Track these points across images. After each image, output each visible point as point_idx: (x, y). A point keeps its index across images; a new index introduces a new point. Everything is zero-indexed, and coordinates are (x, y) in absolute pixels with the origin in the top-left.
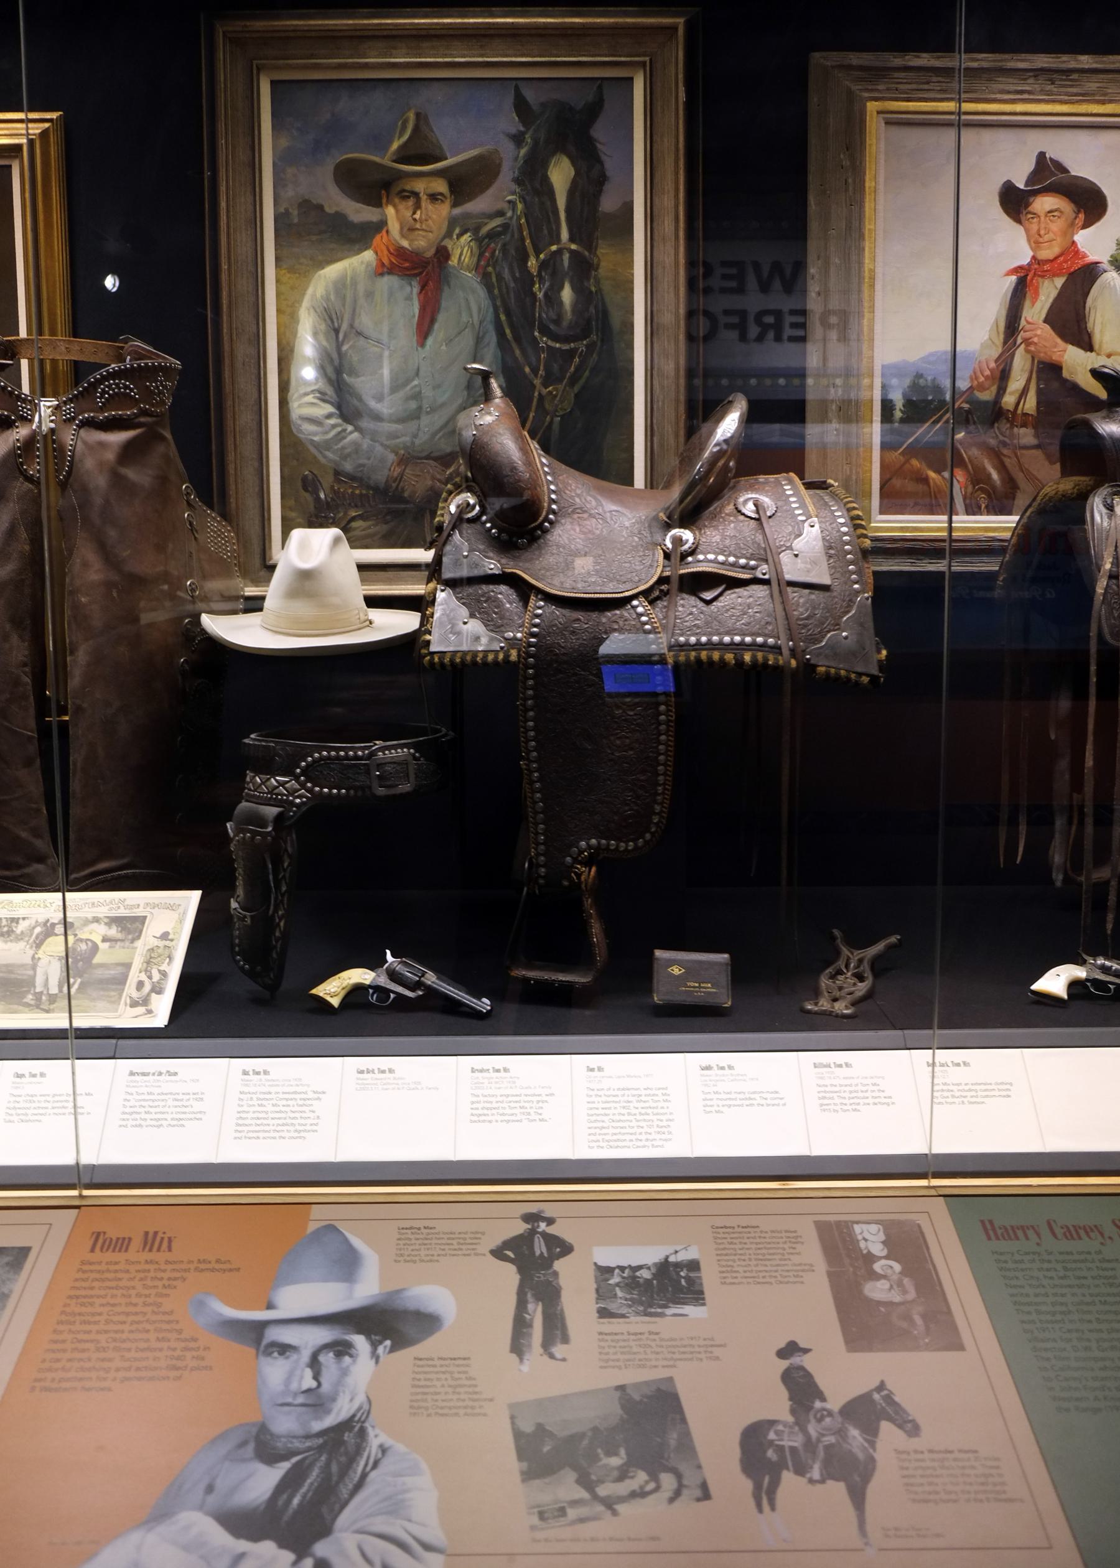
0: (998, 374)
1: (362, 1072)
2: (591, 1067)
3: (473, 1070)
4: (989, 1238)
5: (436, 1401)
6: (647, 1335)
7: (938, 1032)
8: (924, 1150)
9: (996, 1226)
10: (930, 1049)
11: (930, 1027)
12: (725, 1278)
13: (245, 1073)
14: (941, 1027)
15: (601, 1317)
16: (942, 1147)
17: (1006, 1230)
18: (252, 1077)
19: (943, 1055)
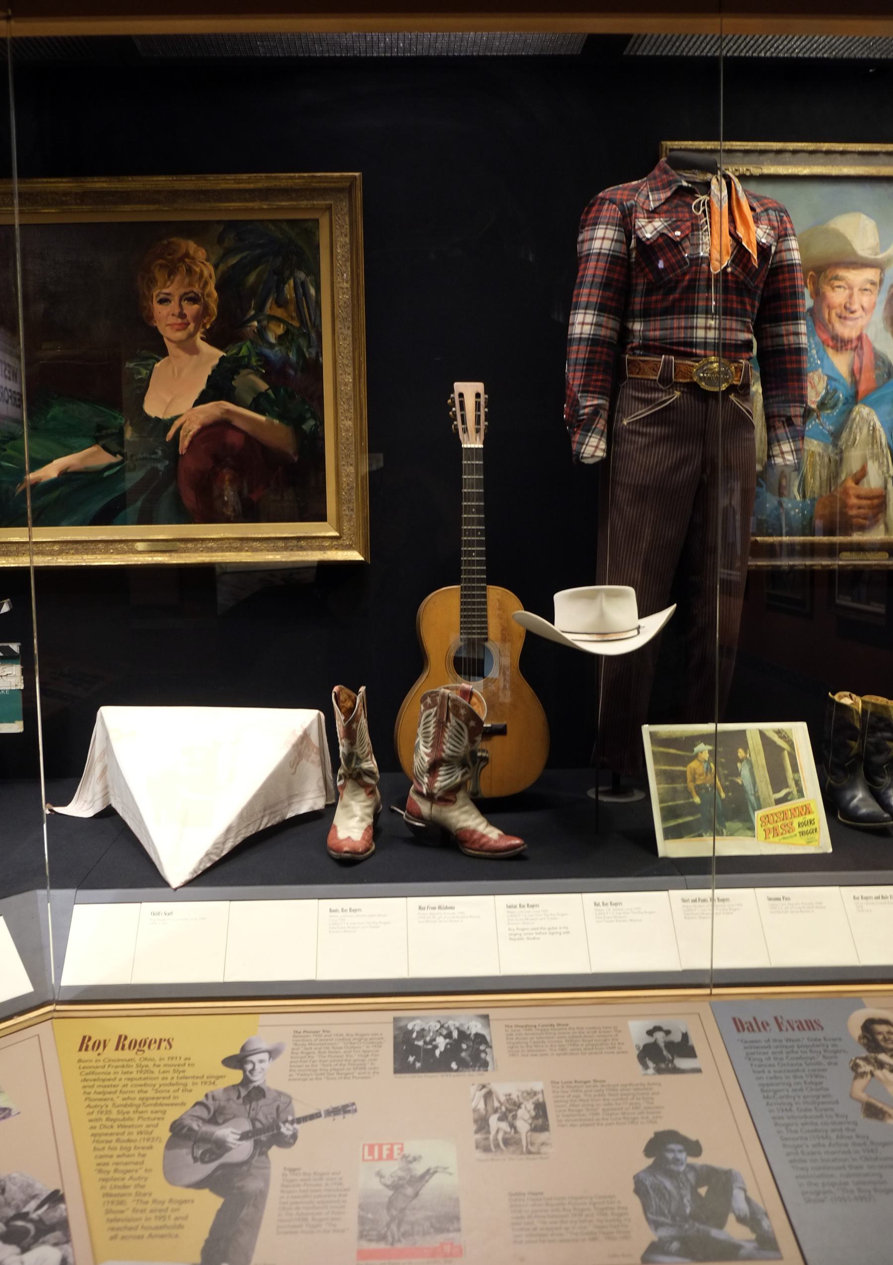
0: (667, 215)
1: (510, 907)
2: (597, 902)
3: (596, 904)
4: (738, 1030)
5: (89, 1093)
6: (592, 1083)
7: (716, 877)
8: (706, 965)
9: (744, 1023)
10: (710, 888)
11: (710, 873)
12: (297, 1041)
13: (596, 904)
14: (718, 873)
15: (402, 1067)
16: (722, 963)
17: (801, 1023)
18: (602, 907)
19: (720, 893)
